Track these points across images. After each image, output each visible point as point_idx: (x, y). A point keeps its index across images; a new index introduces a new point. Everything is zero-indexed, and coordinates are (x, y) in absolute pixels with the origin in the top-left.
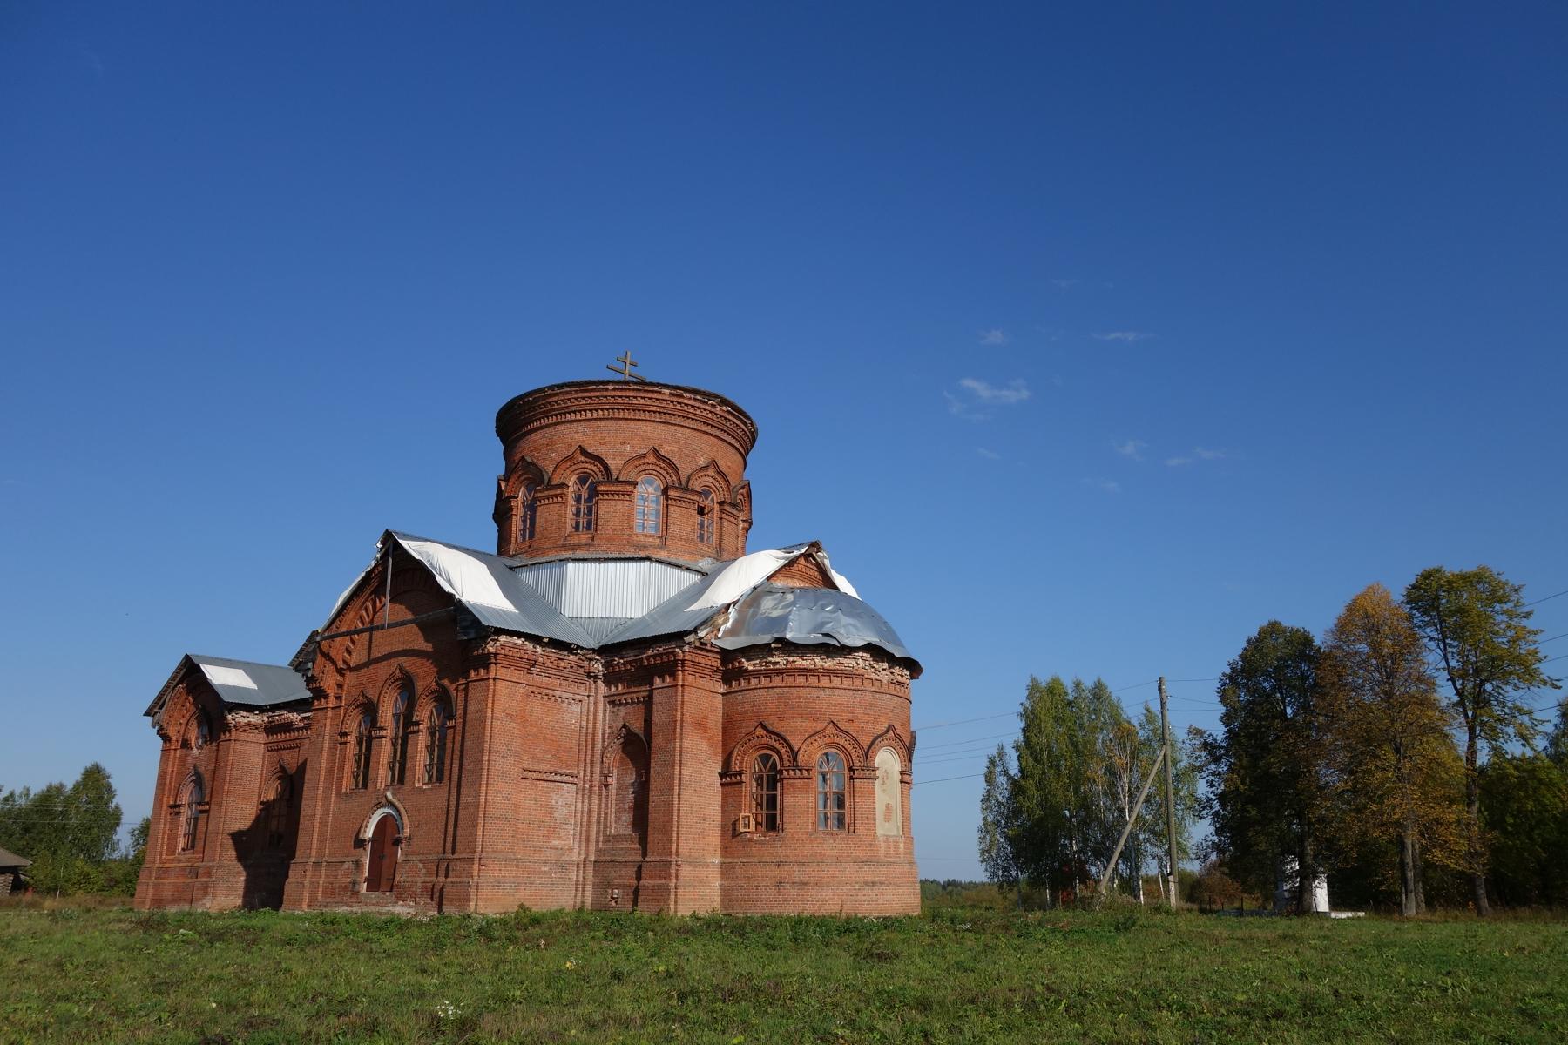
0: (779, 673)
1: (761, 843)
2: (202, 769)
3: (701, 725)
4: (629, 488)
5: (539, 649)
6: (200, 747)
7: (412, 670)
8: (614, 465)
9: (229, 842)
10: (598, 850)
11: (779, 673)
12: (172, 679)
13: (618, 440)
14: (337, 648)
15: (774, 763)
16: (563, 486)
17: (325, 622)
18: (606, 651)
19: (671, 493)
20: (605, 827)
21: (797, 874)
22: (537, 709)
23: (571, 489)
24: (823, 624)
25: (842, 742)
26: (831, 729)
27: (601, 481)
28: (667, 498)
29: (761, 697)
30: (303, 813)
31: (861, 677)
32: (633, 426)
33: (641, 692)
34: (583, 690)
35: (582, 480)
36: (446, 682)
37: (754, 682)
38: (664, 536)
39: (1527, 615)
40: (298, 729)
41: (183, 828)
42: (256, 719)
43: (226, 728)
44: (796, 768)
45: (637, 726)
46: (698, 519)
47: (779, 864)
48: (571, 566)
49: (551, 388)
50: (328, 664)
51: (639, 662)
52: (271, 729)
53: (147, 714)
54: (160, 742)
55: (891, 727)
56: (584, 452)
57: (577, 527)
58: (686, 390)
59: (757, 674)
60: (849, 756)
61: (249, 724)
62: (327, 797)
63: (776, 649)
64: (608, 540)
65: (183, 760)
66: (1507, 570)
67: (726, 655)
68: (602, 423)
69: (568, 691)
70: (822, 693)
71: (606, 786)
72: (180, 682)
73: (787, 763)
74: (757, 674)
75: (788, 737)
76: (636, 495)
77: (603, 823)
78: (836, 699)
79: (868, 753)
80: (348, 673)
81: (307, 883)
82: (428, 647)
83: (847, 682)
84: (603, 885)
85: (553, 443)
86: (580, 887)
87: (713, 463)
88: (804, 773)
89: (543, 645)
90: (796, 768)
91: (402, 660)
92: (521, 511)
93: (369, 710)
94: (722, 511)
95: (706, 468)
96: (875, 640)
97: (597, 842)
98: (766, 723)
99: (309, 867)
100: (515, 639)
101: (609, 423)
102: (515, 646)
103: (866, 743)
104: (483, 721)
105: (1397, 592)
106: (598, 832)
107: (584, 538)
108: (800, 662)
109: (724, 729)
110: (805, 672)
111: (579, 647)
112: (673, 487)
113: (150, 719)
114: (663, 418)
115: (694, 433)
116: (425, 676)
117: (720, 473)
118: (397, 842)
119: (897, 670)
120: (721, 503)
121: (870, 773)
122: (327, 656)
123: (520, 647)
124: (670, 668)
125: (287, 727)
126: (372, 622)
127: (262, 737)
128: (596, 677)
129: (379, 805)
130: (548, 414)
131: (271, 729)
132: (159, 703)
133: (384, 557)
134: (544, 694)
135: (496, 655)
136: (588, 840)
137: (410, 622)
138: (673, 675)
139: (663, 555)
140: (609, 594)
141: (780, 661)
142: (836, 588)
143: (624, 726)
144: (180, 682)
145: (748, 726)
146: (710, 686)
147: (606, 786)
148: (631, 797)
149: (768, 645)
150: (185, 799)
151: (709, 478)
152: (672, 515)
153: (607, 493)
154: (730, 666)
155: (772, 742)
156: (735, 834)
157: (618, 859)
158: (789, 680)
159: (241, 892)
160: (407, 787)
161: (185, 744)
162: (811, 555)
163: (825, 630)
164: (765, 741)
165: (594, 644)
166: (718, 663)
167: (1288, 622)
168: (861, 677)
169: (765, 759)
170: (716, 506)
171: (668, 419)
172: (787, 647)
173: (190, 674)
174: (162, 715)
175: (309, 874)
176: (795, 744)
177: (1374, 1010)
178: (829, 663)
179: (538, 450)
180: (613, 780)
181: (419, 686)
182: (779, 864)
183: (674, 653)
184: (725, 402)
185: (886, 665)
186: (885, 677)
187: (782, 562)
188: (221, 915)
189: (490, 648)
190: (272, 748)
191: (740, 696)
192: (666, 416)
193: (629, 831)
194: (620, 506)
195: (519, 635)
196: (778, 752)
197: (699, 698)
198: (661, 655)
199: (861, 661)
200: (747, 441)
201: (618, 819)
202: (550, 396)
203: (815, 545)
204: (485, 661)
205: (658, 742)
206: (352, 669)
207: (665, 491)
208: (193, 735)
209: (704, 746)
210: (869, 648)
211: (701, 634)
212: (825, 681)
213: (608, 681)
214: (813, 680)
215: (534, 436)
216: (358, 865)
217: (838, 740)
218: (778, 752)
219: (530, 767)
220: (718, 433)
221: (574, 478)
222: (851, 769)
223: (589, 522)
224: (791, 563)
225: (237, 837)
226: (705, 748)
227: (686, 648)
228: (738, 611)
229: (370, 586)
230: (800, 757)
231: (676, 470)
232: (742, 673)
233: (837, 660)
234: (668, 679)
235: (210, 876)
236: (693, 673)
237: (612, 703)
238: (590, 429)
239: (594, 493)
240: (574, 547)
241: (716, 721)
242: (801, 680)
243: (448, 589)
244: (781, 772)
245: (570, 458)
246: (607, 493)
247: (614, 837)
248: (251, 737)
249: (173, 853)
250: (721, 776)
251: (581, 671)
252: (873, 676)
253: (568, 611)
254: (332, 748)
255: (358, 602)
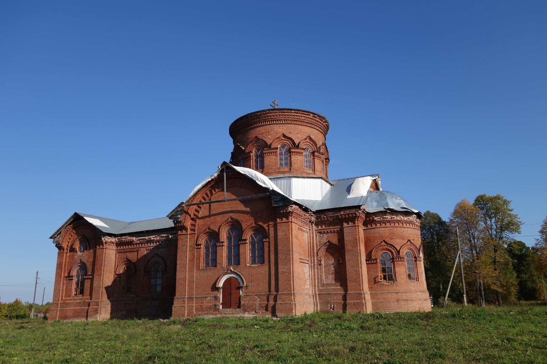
0: (389, 222)
1: (389, 285)
2: (85, 261)
6: (81, 252)
7: (239, 219)
9: (104, 291)
10: (319, 289)
12: (66, 223)
14: (192, 210)
17: (187, 198)
19: (316, 154)
20: (321, 280)
21: (404, 296)
29: (382, 231)
30: (177, 277)
32: (300, 127)
33: (337, 228)
39: (511, 210)
40: (136, 244)
41: (74, 286)
42: (113, 240)
43: (101, 243)
45: (334, 240)
47: (397, 293)
48: (294, 180)
52: (118, 244)
53: (51, 238)
54: (57, 250)
56: (284, 136)
57: (281, 164)
59: (380, 222)
61: (111, 241)
62: (191, 271)
63: (389, 213)
65: (72, 257)
66: (506, 196)
68: (289, 125)
71: (320, 265)
72: (70, 224)
74: (380, 222)
77: (320, 279)
80: (198, 220)
81: (186, 307)
82: (248, 209)
84: (325, 302)
86: (315, 304)
88: (402, 259)
91: (231, 214)
92: (254, 158)
93: (214, 236)
97: (318, 287)
99: (186, 300)
101: (292, 125)
105: (471, 201)
106: (318, 283)
108: (395, 218)
110: (398, 222)
113: (52, 240)
116: (247, 222)
118: (239, 288)
122: (187, 213)
125: (131, 243)
126: (210, 199)
127: (114, 247)
129: (226, 273)
130: (266, 121)
131: (118, 244)
132: (58, 233)
133: (222, 171)
135: (292, 212)
136: (315, 285)
137: (235, 200)
141: (388, 217)
144: (70, 224)
147: (320, 265)
148: (333, 269)
150: (74, 273)
152: (316, 162)
153: (294, 152)
155: (389, 248)
156: (375, 282)
157: (331, 293)
159: (110, 312)
160: (242, 265)
161: (72, 250)
165: (314, 209)
167: (432, 211)
173: (77, 222)
174: (59, 238)
175: (186, 302)
177: (470, 336)
178: (406, 218)
180: (323, 262)
181: (244, 226)
182: (397, 293)
183: (355, 213)
188: (208, 320)
189: (290, 209)
190: (119, 252)
193: (334, 282)
198: (348, 214)
201: (327, 278)
202: (268, 113)
204: (287, 215)
205: (348, 247)
206: (199, 218)
208: (77, 246)
213: (317, 225)
214: (392, 225)
215: (258, 129)
216: (216, 298)
225: (107, 288)
229: (214, 185)
230: (401, 254)
232: (373, 221)
235: (98, 305)
237: (320, 233)
239: (289, 151)
240: (284, 173)
243: (264, 186)
245: (279, 138)
247: (327, 284)
248: (111, 247)
249: (70, 296)
254: (192, 250)
255: (205, 189)
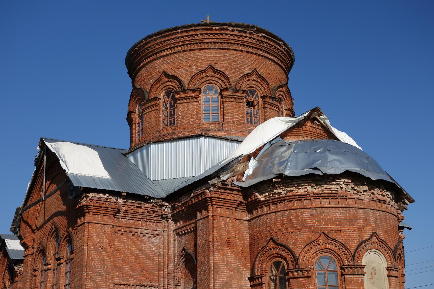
3: (229, 243)
4: (196, 94)
5: (121, 201)
8: (185, 80)
11: (282, 200)
13: (184, 64)
15: (283, 267)
16: (156, 98)
17: (23, 202)
18: (172, 198)
19: (224, 93)
22: (124, 243)
23: (162, 100)
24: (314, 162)
25: (333, 247)
26: (323, 239)
27: (179, 91)
28: (222, 98)
29: (272, 218)
31: (344, 197)
32: (197, 53)
34: (160, 227)
35: (168, 94)
36: (70, 229)
37: (266, 209)
38: (222, 123)
44: (298, 269)
45: (190, 250)
46: (247, 109)
49: (146, 39)
50: (28, 228)
51: (189, 201)
55: (374, 234)
56: (167, 75)
58: (230, 25)
59: (267, 203)
60: (339, 257)
64: (184, 129)
67: (245, 192)
69: (148, 228)
70: (314, 212)
73: (291, 267)
74: (267, 203)
75: (292, 247)
76: (202, 98)
78: (326, 214)
79: (355, 256)
83: (333, 203)
85: (150, 73)
87: (255, 71)
89: (124, 198)
90: (298, 269)
94: (265, 102)
95: (249, 75)
96: (354, 168)
98: (276, 238)
100: (101, 195)
101: (181, 54)
102: (100, 199)
103: (352, 247)
104: (82, 252)
107: (170, 130)
108: (296, 191)
109: (250, 245)
110: (300, 197)
111: (151, 198)
112: (227, 89)
114: (217, 46)
115: (240, 53)
117: (260, 77)
119: (377, 191)
120: (263, 97)
121: (358, 270)
123: (104, 200)
124: (203, 205)
128: (167, 218)
134: (129, 232)
135: (87, 206)
138: (206, 209)
139: (221, 134)
140: (173, 163)
141: (282, 191)
142: (340, 141)
143: (184, 249)
145: (263, 242)
146: (237, 215)
149: (271, 180)
151: (253, 81)
152: (226, 107)
153: (182, 99)
154: (249, 198)
158: (289, 205)
162: (315, 119)
163: (314, 166)
164: (276, 251)
165: (164, 195)
166: (241, 198)
168: (344, 197)
169: (277, 265)
170: (260, 100)
171: (220, 46)
172: (285, 181)
176: (296, 251)
178: (319, 190)
179: (143, 80)
183: (204, 193)
184: (260, 31)
185: (366, 188)
186: (366, 197)
187: (290, 125)
189: (84, 202)
191: (258, 221)
192: (219, 44)
194: (191, 106)
195: (104, 192)
196: (285, 259)
197: (227, 224)
199: (343, 186)
200: (287, 62)
202: (146, 44)
203: (315, 110)
204: (82, 212)
205: (200, 258)
207: (221, 94)
209: (233, 258)
210: (347, 174)
211: (224, 177)
212: (316, 203)
217: (329, 246)
218: (285, 259)
219: (121, 282)
220: (258, 52)
221: (163, 93)
222: (342, 268)
223: (173, 119)
224: (299, 125)
226: (234, 260)
227: (212, 189)
228: (259, 161)
230: (300, 262)
231: (227, 78)
233: (324, 187)
234: (204, 212)
236: (221, 207)
237: (178, 234)
238: (170, 60)
241: (243, 240)
242: (298, 204)
243: (64, 167)
244: (287, 274)
246: (182, 99)
250: (251, 279)
251: (156, 214)
252: (356, 196)
253: (152, 176)
254: (31, 280)
